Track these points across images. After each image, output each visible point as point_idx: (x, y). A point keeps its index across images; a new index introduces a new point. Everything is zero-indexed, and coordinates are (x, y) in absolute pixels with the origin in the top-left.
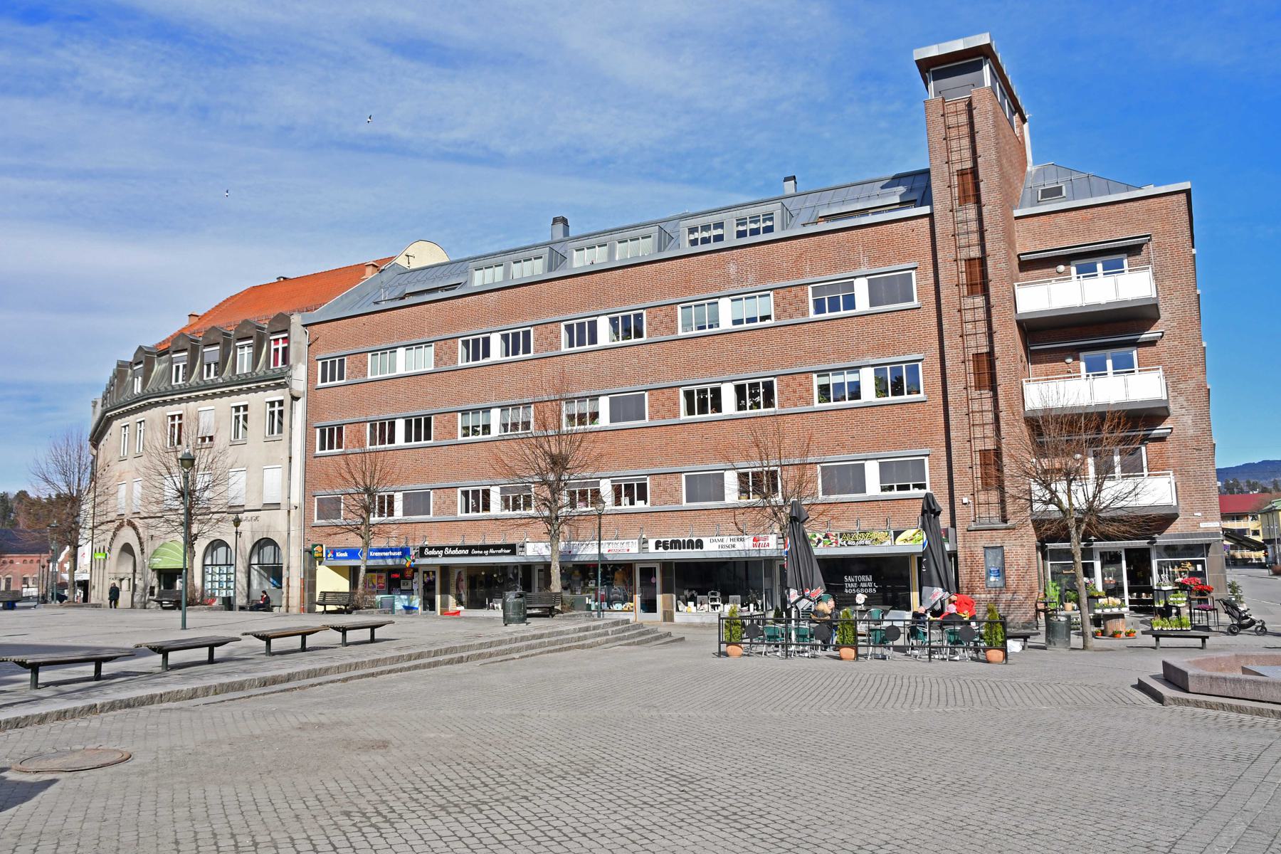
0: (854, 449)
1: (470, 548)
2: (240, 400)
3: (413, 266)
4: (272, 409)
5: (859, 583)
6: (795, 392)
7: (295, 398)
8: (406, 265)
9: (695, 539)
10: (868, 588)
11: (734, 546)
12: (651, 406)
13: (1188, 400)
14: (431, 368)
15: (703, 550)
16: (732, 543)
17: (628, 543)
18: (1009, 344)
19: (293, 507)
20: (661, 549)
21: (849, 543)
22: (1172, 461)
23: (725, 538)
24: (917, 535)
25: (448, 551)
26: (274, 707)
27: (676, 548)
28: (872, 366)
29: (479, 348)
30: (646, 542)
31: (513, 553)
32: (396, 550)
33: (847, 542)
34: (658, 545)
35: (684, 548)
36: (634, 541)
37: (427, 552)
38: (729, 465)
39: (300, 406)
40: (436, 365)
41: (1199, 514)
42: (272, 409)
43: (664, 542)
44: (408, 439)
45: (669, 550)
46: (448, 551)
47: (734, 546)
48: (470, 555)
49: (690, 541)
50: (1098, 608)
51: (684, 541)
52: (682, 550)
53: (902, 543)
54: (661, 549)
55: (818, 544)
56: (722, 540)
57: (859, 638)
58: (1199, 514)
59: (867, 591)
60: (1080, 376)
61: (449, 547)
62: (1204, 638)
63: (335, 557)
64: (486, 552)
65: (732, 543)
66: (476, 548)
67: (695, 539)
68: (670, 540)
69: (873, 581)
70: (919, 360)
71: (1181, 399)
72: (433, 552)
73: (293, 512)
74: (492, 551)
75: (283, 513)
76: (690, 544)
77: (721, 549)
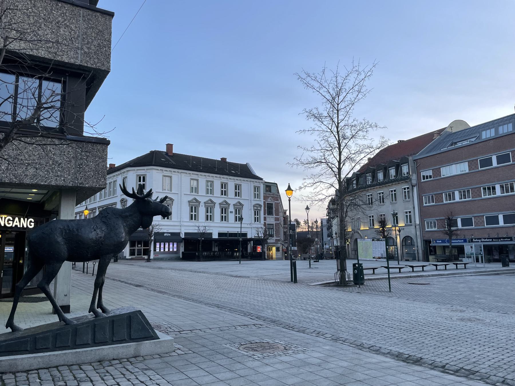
0: (495, 211)
1: (492, 239)
2: (229, 212)
4: (392, 193)
6: (476, 193)
7: (413, 186)
8: (451, 131)
25: (483, 240)
31: (511, 240)
32: (461, 240)
37: (474, 240)
39: (415, 189)
40: (469, 170)
42: (392, 193)
46: (483, 240)
48: (492, 241)
57: (171, 250)
61: (483, 238)
63: (436, 242)
64: (500, 240)
66: (495, 238)
73: (417, 227)
74: (502, 240)
75: (413, 227)
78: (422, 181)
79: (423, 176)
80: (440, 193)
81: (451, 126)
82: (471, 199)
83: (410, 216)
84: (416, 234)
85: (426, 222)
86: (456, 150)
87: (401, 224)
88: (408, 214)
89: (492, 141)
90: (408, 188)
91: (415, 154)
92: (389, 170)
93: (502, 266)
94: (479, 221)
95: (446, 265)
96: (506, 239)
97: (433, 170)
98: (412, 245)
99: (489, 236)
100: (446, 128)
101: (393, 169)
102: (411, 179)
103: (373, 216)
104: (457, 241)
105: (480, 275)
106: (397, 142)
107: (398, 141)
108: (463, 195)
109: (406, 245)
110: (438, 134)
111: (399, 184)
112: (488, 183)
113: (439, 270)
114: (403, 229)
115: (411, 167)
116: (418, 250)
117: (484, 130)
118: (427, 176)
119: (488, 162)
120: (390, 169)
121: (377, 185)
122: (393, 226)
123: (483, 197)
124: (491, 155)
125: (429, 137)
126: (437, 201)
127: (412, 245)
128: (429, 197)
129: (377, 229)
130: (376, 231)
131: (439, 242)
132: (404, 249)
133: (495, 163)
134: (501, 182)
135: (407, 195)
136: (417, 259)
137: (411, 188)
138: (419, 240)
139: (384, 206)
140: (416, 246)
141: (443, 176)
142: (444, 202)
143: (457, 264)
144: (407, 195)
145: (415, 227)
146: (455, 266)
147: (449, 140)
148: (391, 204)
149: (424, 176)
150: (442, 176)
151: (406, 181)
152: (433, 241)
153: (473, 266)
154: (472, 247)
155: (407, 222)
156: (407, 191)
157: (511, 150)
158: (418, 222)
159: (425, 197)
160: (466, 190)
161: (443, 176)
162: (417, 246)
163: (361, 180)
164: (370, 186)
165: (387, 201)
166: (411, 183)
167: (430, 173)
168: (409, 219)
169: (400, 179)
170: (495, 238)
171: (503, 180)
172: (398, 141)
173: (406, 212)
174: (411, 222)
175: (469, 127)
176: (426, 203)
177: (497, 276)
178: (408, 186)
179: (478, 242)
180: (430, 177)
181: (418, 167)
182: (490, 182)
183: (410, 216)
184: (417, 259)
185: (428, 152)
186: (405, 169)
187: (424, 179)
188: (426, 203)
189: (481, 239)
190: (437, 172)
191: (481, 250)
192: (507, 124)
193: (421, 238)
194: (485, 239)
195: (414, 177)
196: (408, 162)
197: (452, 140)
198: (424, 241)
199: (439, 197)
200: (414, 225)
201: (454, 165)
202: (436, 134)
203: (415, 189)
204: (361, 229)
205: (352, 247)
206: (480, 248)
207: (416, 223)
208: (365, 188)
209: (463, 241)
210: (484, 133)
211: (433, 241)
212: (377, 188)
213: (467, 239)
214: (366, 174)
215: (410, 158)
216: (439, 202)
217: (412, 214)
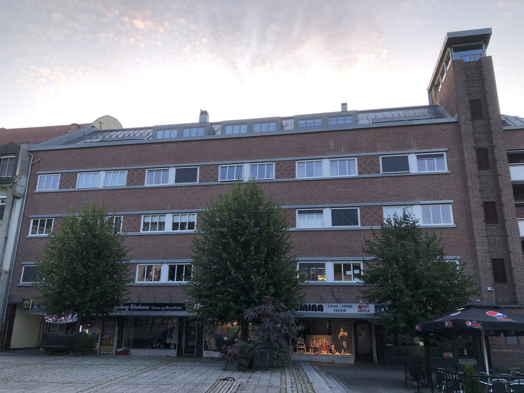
7: (16, 197)
9: (317, 305)
11: (345, 311)
14: (57, 189)
16: (344, 308)
25: (132, 307)
39: (18, 204)
40: (128, 184)
46: (132, 307)
48: (150, 310)
49: (314, 306)
51: (310, 305)
52: (308, 312)
56: (337, 306)
64: (163, 308)
65: (344, 308)
67: (317, 305)
74: (167, 308)
76: (314, 308)
77: (336, 312)
179: (124, 310)
203: (18, 204)
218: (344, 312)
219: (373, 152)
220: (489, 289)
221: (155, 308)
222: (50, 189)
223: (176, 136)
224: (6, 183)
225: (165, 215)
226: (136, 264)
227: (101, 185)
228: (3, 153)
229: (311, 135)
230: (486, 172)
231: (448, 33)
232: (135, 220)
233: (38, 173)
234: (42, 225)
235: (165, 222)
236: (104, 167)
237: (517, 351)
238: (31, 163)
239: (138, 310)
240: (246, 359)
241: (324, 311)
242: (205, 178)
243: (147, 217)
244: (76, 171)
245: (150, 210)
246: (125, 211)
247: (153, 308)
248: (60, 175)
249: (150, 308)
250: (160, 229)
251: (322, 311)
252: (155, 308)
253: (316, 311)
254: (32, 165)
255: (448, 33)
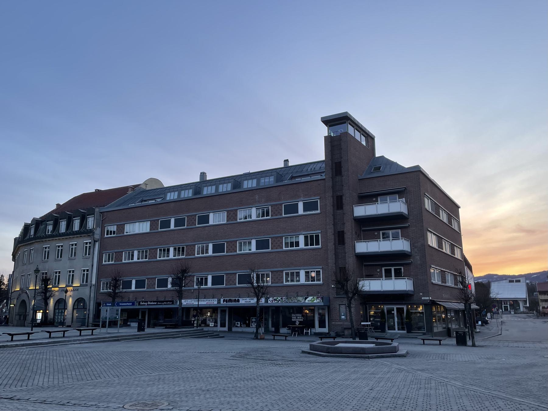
3: (148, 189)
5: (297, 317)
6: (231, 247)
7: (95, 241)
8: (145, 188)
9: (237, 299)
10: (300, 319)
11: (250, 302)
12: (227, 247)
13: (418, 250)
14: (225, 222)
15: (240, 303)
16: (250, 300)
17: (214, 300)
18: (349, 229)
19: (92, 285)
20: (225, 303)
21: (290, 301)
22: (412, 273)
23: (247, 299)
24: (313, 299)
25: (149, 303)
26: (38, 349)
27: (230, 302)
28: (303, 234)
29: (166, 224)
30: (220, 300)
31: (173, 304)
33: (289, 301)
34: (224, 301)
35: (233, 302)
36: (216, 299)
38: (169, 276)
39: (97, 245)
40: (150, 230)
41: (422, 294)
43: (226, 300)
44: (306, 244)
45: (228, 303)
46: (149, 303)
47: (250, 302)
48: (157, 304)
49: (235, 300)
50: (61, 314)
51: (233, 299)
52: (232, 303)
53: (308, 302)
54: (225, 303)
55: (279, 301)
56: (246, 299)
58: (422, 294)
59: (299, 320)
60: (390, 240)
62: (440, 341)
63: (139, 304)
64: (163, 303)
65: (250, 300)
67: (237, 299)
68: (228, 299)
69: (302, 316)
70: (319, 233)
71: (416, 250)
72: (144, 303)
73: (92, 288)
74: (165, 303)
76: (235, 301)
77: (245, 303)
78: (106, 236)
79: (107, 230)
80: (120, 252)
81: (145, 184)
82: (147, 260)
83: (87, 274)
84: (90, 296)
85: (102, 283)
86: (152, 206)
87: (76, 284)
88: (86, 273)
89: (173, 204)
90: (90, 243)
91: (104, 206)
92: (73, 220)
93: (137, 331)
94: (151, 283)
95: (64, 331)
96: (168, 303)
97: (228, 211)
98: (84, 308)
99: (157, 299)
100: (141, 184)
101: (78, 219)
102: (94, 233)
103: (59, 272)
104: (126, 304)
105: (94, 342)
106: (95, 191)
107: (96, 190)
108: (178, 250)
109: (77, 308)
110: (133, 189)
111: (81, 237)
112: (164, 245)
113: (426, 344)
114: (78, 289)
115: (96, 219)
116: (89, 315)
117: (206, 186)
118: (111, 232)
119: (295, 208)
120: (75, 220)
121: (57, 236)
122: (67, 286)
123: (284, 248)
124: (209, 212)
125: (123, 191)
126: (117, 259)
127: (84, 308)
128: (109, 255)
129: (62, 289)
130: (62, 290)
131: (109, 305)
132: (75, 311)
133: (301, 211)
134: (174, 245)
135: (88, 251)
136: (86, 324)
137: (93, 243)
138: (92, 303)
139: (61, 261)
140: (88, 309)
141: (126, 233)
142: (238, 252)
143: (80, 330)
144: (88, 251)
145: (91, 287)
146: (78, 333)
147: (141, 197)
148: (70, 259)
149: (108, 231)
150: (125, 234)
151: (89, 234)
152: (103, 304)
153: (72, 333)
154: (107, 311)
155: (83, 281)
156: (75, 248)
157: (187, 215)
158: (94, 282)
159: (106, 255)
160: (144, 250)
161: (126, 233)
162: (89, 310)
163: (42, 227)
164: (50, 236)
165: (66, 256)
166: (94, 238)
167: (114, 228)
168: (86, 278)
169: (84, 232)
170: (160, 302)
171: (177, 244)
172: (96, 190)
173: (84, 271)
174: (87, 282)
175: (163, 187)
176: (105, 261)
177: (116, 342)
178: (90, 241)
179: (145, 305)
180: (114, 233)
181: (102, 223)
182: (166, 244)
183: (87, 274)
184: (86, 324)
185: (119, 205)
186: (91, 223)
187: (107, 234)
188: (105, 261)
189: (147, 302)
190: (121, 228)
191: (117, 314)
192: (227, 183)
193: (94, 301)
194: (151, 302)
195: (98, 232)
196: (94, 214)
197: (143, 197)
198: (97, 304)
199: (119, 257)
200: (89, 285)
201: (137, 224)
202: (131, 188)
203: (97, 245)
204: (30, 288)
205: (17, 311)
206: (117, 311)
207: (92, 283)
208: (43, 238)
209: (131, 304)
210: (169, 194)
211: (103, 304)
212: (56, 239)
213: (174, 301)
214: (47, 221)
215: (97, 210)
216: (118, 261)
217: (89, 273)
218: (250, 303)
219: (279, 201)
220: (333, 286)
221: (160, 303)
222: (144, 231)
223: (255, 186)
224: (90, 233)
225: (299, 236)
226: (156, 278)
227: (137, 232)
228: (88, 214)
229: (247, 192)
230: (340, 211)
231: (321, 118)
232: (233, 245)
233: (105, 225)
234: (179, 251)
235: (299, 242)
236: (138, 220)
237: (345, 323)
238: (101, 220)
239: (153, 305)
240: (119, 330)
241: (240, 303)
242: (193, 223)
243: (297, 237)
244: (236, 208)
245: (161, 245)
246: (150, 246)
247: (158, 303)
248: (150, 221)
249: (157, 303)
250: (108, 262)
251: (239, 302)
252: (160, 303)
253: (236, 302)
254: (102, 221)
255: (321, 118)
